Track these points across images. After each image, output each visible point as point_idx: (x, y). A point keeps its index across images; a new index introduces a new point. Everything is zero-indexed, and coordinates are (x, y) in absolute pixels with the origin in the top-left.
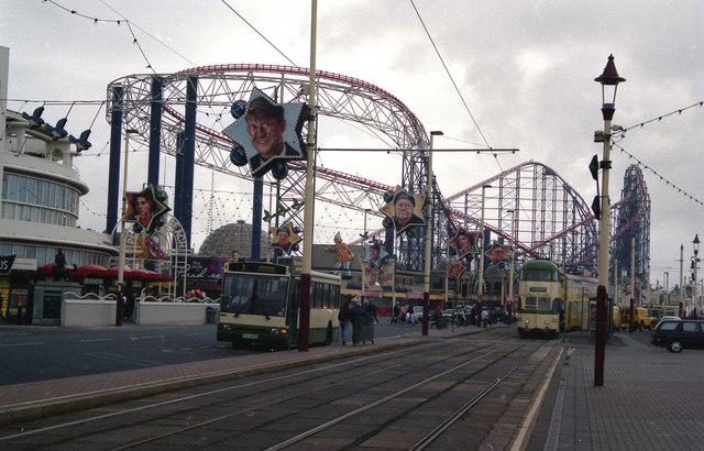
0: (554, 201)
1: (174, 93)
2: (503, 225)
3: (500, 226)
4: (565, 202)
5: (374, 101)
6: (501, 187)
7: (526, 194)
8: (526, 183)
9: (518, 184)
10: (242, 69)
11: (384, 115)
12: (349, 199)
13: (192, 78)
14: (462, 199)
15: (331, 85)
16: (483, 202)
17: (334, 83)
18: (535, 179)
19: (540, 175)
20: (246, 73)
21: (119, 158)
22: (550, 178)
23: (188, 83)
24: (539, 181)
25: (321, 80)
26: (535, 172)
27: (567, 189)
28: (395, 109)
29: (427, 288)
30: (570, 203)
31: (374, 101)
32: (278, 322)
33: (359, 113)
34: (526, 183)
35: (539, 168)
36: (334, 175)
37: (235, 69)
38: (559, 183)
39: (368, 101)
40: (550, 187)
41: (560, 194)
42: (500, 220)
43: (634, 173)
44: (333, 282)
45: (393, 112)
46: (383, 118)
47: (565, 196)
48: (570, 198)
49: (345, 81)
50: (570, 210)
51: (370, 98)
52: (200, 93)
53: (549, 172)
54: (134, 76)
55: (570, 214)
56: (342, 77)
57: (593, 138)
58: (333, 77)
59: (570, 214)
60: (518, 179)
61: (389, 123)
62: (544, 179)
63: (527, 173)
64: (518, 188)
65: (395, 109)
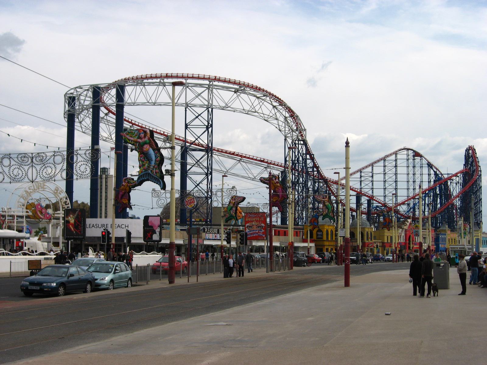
1: (110, 98)
2: (387, 200)
4: (429, 175)
5: (258, 98)
7: (402, 170)
8: (402, 163)
10: (156, 77)
11: (267, 108)
12: (252, 174)
13: (120, 87)
15: (223, 87)
17: (226, 85)
18: (408, 160)
19: (411, 157)
20: (158, 80)
22: (418, 159)
23: (117, 91)
24: (411, 161)
25: (216, 83)
26: (408, 155)
27: (430, 166)
28: (275, 104)
31: (258, 98)
32: (204, 223)
33: (247, 108)
34: (402, 163)
35: (410, 152)
36: (241, 156)
37: (151, 78)
38: (424, 162)
39: (253, 98)
41: (425, 170)
42: (385, 196)
43: (471, 152)
44: (293, 264)
45: (274, 107)
46: (267, 112)
47: (429, 170)
49: (235, 83)
51: (255, 96)
52: (126, 97)
53: (417, 154)
54: (80, 87)
56: (227, 80)
58: (225, 81)
60: (396, 160)
61: (271, 115)
62: (414, 159)
63: (402, 156)
65: (275, 104)
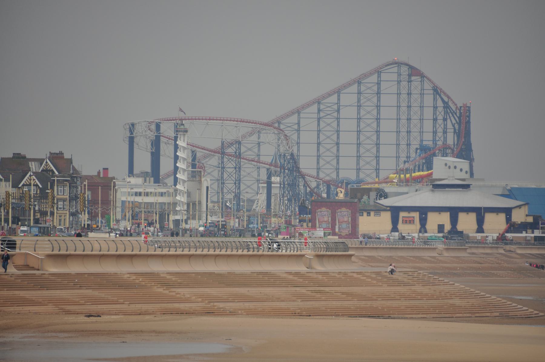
0: (421, 120)
3: (358, 176)
4: (435, 108)
6: (359, 93)
9: (379, 88)
14: (314, 108)
16: (338, 111)
18: (399, 82)
19: (404, 77)
21: (20, 183)
24: (404, 84)
27: (436, 91)
29: (202, 170)
30: (440, 109)
35: (405, 70)
38: (427, 86)
40: (416, 91)
41: (429, 100)
47: (435, 99)
48: (440, 103)
50: (440, 117)
53: (414, 72)
55: (440, 122)
57: (369, 217)
59: (440, 122)
60: (379, 84)
62: (410, 81)
64: (378, 93)
